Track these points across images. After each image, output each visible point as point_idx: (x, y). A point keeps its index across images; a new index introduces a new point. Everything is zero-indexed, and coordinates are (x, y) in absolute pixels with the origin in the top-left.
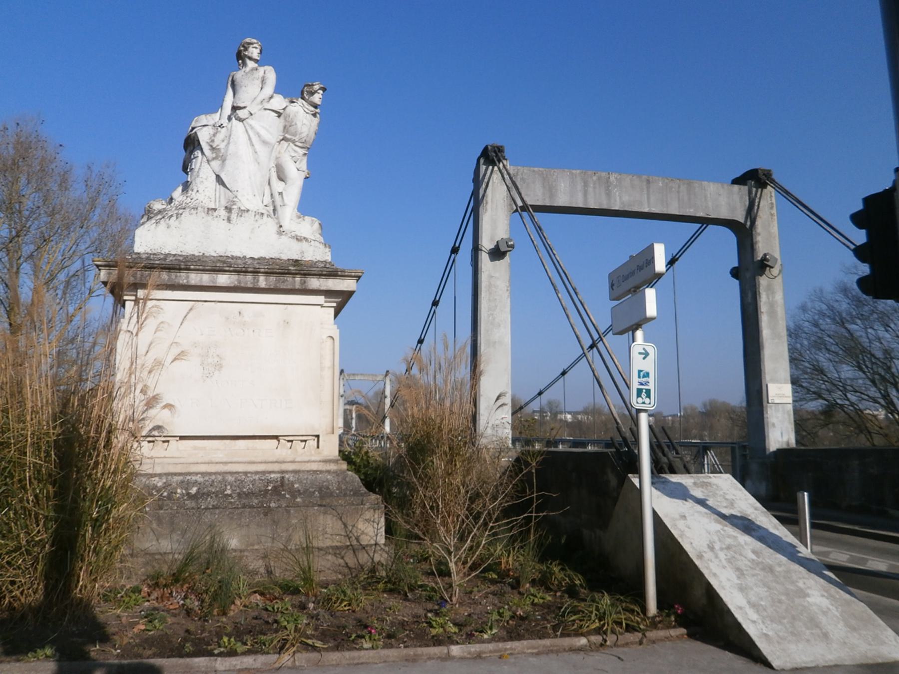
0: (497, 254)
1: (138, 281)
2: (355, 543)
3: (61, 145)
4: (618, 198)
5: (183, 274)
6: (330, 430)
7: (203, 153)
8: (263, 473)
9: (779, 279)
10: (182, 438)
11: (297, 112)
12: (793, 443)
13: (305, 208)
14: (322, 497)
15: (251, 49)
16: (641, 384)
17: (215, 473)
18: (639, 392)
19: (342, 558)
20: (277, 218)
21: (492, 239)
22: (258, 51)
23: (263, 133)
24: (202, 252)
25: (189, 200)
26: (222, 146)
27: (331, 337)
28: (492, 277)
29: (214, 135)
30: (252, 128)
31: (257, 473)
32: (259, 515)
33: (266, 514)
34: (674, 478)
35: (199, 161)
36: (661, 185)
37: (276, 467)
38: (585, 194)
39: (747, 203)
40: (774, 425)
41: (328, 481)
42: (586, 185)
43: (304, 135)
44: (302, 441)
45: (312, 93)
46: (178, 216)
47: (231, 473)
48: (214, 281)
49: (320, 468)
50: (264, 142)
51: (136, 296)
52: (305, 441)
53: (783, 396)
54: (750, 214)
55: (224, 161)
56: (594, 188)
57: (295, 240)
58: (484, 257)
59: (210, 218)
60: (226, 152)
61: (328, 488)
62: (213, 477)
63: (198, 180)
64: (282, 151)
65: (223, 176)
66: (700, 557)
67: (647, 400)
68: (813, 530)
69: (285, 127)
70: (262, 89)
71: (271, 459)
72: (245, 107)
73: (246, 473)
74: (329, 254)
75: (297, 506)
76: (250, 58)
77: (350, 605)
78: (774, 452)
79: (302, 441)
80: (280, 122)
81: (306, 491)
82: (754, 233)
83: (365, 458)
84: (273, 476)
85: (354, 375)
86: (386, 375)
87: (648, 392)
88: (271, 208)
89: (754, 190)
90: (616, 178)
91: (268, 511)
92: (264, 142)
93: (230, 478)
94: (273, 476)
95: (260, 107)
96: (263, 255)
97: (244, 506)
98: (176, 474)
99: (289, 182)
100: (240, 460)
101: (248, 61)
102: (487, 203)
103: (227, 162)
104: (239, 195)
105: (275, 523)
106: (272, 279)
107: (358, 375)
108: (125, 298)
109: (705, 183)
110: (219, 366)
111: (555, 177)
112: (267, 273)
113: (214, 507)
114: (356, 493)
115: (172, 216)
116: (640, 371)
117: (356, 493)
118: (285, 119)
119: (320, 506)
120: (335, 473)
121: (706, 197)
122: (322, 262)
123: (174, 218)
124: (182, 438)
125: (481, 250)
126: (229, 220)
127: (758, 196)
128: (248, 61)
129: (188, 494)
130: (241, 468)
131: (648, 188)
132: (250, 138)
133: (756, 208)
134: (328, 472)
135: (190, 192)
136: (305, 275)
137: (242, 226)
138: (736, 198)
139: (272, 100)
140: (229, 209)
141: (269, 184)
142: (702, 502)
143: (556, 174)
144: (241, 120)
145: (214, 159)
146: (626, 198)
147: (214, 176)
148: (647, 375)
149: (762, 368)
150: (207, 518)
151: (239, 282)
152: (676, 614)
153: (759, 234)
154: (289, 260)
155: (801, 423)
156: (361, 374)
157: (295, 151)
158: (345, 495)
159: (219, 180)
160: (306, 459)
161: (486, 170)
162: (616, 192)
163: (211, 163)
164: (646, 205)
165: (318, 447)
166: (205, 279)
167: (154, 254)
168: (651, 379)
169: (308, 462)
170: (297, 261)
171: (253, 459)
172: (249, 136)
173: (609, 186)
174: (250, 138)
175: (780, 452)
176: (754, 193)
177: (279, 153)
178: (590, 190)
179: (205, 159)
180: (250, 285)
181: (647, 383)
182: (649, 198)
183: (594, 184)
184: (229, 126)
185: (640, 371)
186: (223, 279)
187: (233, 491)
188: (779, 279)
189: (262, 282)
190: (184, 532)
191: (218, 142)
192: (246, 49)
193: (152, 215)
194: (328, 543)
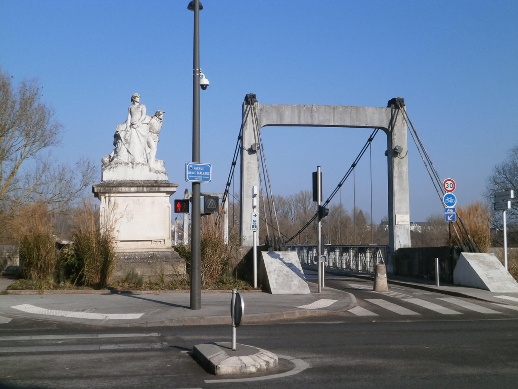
0: (251, 151)
1: (106, 191)
2: (177, 273)
3: (12, 77)
5: (120, 188)
6: (169, 238)
7: (122, 141)
8: (147, 252)
9: (406, 158)
10: (121, 241)
11: (154, 122)
12: (410, 246)
13: (158, 157)
14: (166, 259)
15: (137, 98)
16: (254, 224)
17: (132, 252)
19: (173, 278)
20: (149, 165)
21: (249, 143)
22: (139, 99)
23: (142, 133)
24: (125, 179)
25: (118, 160)
26: (128, 139)
27: (168, 207)
28: (249, 163)
29: (126, 134)
30: (139, 131)
31: (145, 252)
32: (147, 264)
33: (149, 264)
34: (277, 252)
35: (120, 144)
37: (151, 250)
38: (299, 117)
39: (390, 117)
40: (398, 236)
41: (168, 254)
42: (300, 112)
43: (157, 130)
44: (159, 242)
45: (159, 115)
46: (116, 167)
47: (137, 252)
49: (166, 250)
50: (143, 136)
51: (105, 195)
52: (160, 242)
53: (404, 221)
54: (391, 123)
55: (129, 144)
56: (304, 113)
57: (155, 173)
58: (246, 153)
59: (126, 167)
60: (130, 141)
61: (168, 257)
62: (132, 253)
63: (121, 152)
64: (149, 136)
65: (129, 150)
66: (270, 272)
67: (255, 229)
68: (389, 284)
69: (150, 128)
70: (141, 116)
71: (149, 248)
72: (136, 124)
73: (142, 252)
74: (167, 177)
75: (158, 262)
76: (136, 102)
77: (174, 286)
78: (397, 250)
79: (159, 242)
80: (148, 126)
81: (161, 257)
82: (392, 134)
83: (183, 249)
84: (150, 253)
87: (256, 226)
88: (147, 160)
89: (394, 110)
90: (316, 108)
91: (149, 263)
92: (143, 136)
93: (137, 254)
94: (150, 253)
96: (145, 179)
97: (142, 262)
99: (152, 149)
100: (140, 248)
101: (135, 103)
102: (247, 125)
103: (131, 145)
104: (135, 157)
106: (148, 188)
108: (101, 196)
109: (366, 108)
110: (132, 218)
111: (283, 109)
113: (133, 262)
114: (177, 258)
115: (114, 167)
116: (253, 220)
117: (177, 258)
118: (150, 125)
119: (166, 262)
120: (171, 252)
121: (366, 115)
122: (165, 181)
123: (115, 168)
124: (121, 241)
125: (244, 149)
126: (133, 167)
127: (396, 114)
128: (135, 103)
129: (125, 259)
130: (128, 251)
131: (334, 112)
132: (138, 135)
133: (394, 120)
134: (168, 252)
135: (118, 156)
136: (159, 187)
137: (138, 169)
138: (384, 115)
139: (145, 120)
140: (133, 164)
141: (145, 149)
142: (281, 259)
143: (283, 107)
144: (135, 128)
145: (126, 143)
146: (321, 118)
147: (126, 150)
148: (256, 221)
149: (394, 206)
150: (132, 265)
151: (138, 190)
152: (261, 287)
153: (395, 134)
154: (153, 180)
155: (414, 235)
157: (154, 136)
158: (174, 258)
159: (128, 151)
160: (161, 247)
161: (247, 108)
162: (316, 115)
163: (125, 145)
164: (333, 122)
165: (165, 244)
166: (127, 189)
167: (109, 181)
169: (162, 248)
170: (156, 181)
171: (144, 248)
172: (138, 134)
173: (312, 112)
174: (138, 135)
175: (401, 250)
176: (394, 112)
177: (148, 137)
178: (302, 115)
179: (123, 144)
180: (141, 191)
181: (255, 224)
182: (334, 117)
183: (304, 111)
184: (130, 131)
185: (253, 220)
186: (133, 189)
187: (138, 257)
188: (406, 158)
191: (127, 137)
192: (135, 98)
193: (106, 166)
194: (169, 273)
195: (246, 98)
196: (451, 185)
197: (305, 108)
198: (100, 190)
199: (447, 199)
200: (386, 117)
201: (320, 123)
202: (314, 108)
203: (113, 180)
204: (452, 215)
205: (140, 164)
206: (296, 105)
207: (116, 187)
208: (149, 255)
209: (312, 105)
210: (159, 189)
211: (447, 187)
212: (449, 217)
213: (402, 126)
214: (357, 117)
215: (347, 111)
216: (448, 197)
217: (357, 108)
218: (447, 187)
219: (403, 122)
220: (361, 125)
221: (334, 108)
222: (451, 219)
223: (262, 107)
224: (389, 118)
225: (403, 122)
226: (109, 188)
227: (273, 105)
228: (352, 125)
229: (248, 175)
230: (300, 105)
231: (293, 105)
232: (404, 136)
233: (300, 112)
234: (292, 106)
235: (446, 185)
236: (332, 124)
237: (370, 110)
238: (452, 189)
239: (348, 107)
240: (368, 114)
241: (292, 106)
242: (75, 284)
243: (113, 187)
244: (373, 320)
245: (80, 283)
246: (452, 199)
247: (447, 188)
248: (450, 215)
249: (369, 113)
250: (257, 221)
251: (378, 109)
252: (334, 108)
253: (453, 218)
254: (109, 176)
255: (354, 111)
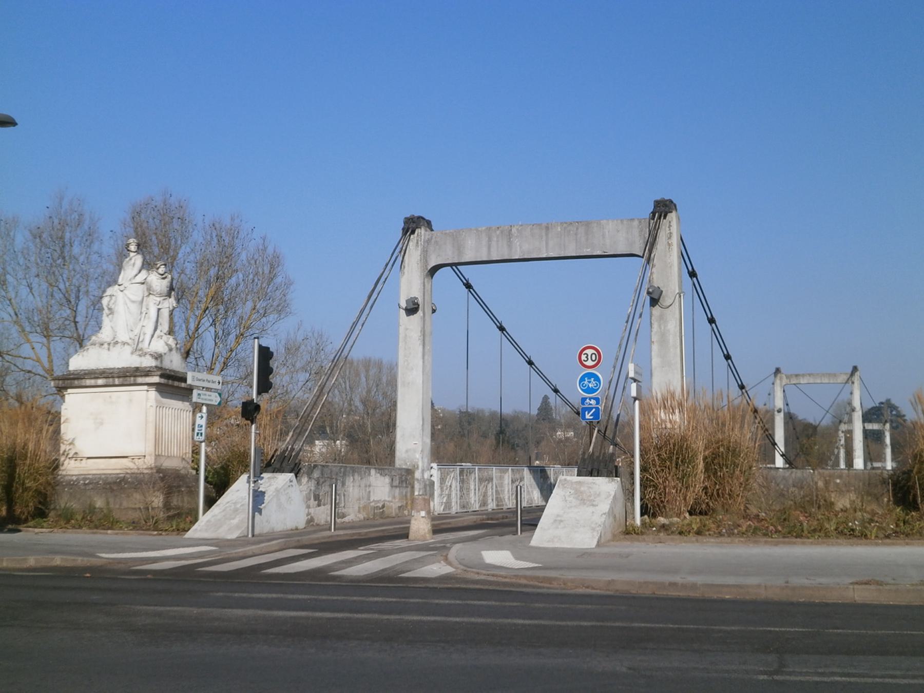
4: (518, 248)
5: (83, 381)
18: (198, 434)
29: (110, 300)
36: (559, 230)
42: (490, 240)
43: (158, 291)
48: (96, 383)
50: (133, 302)
56: (498, 241)
73: (110, 474)
80: (144, 287)
85: (797, 376)
86: (852, 374)
87: (201, 434)
90: (518, 229)
95: (130, 282)
98: (82, 475)
105: (116, 496)
107: (803, 375)
109: (604, 222)
110: (102, 424)
112: (119, 377)
113: (92, 489)
121: (604, 236)
130: (94, 472)
131: (547, 235)
138: (636, 232)
143: (464, 233)
148: (201, 426)
156: (810, 375)
162: (516, 242)
164: (545, 251)
166: (92, 382)
168: (204, 428)
173: (510, 238)
178: (494, 243)
180: (132, 382)
182: (547, 244)
186: (100, 382)
189: (117, 381)
190: (79, 500)
191: (111, 306)
195: (658, 204)
196: (594, 356)
197: (498, 232)
198: (59, 383)
199: (585, 381)
200: (640, 236)
201: (524, 255)
202: (514, 230)
203: (81, 369)
204: (594, 410)
205: (119, 344)
206: (484, 228)
207: (78, 379)
208: (119, 478)
209: (511, 226)
210: (135, 380)
211: (586, 359)
212: (588, 414)
213: (667, 249)
214: (587, 240)
215: (570, 231)
216: (586, 379)
217: (588, 224)
218: (586, 359)
219: (668, 242)
220: (594, 254)
221: (547, 228)
222: (591, 417)
223: (430, 237)
224: (645, 238)
225: (668, 242)
226: (69, 381)
227: (448, 232)
228: (578, 255)
229: (405, 349)
230: (490, 228)
231: (480, 229)
232: (671, 267)
233: (490, 240)
234: (477, 230)
235: (583, 357)
236: (544, 256)
237: (610, 226)
238: (594, 363)
239: (571, 224)
240: (607, 233)
241: (477, 230)
242: (407, 525)
243: (74, 379)
244: (86, 574)
245: (799, 536)
246: (594, 381)
247: (584, 362)
248: (590, 409)
249: (609, 232)
250: (204, 427)
251: (625, 222)
252: (547, 228)
253: (596, 415)
254: (78, 362)
255: (582, 230)
